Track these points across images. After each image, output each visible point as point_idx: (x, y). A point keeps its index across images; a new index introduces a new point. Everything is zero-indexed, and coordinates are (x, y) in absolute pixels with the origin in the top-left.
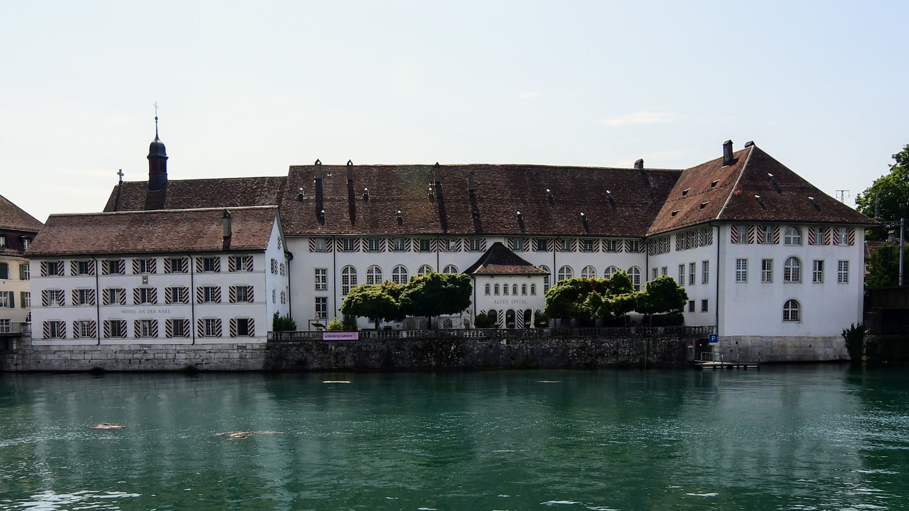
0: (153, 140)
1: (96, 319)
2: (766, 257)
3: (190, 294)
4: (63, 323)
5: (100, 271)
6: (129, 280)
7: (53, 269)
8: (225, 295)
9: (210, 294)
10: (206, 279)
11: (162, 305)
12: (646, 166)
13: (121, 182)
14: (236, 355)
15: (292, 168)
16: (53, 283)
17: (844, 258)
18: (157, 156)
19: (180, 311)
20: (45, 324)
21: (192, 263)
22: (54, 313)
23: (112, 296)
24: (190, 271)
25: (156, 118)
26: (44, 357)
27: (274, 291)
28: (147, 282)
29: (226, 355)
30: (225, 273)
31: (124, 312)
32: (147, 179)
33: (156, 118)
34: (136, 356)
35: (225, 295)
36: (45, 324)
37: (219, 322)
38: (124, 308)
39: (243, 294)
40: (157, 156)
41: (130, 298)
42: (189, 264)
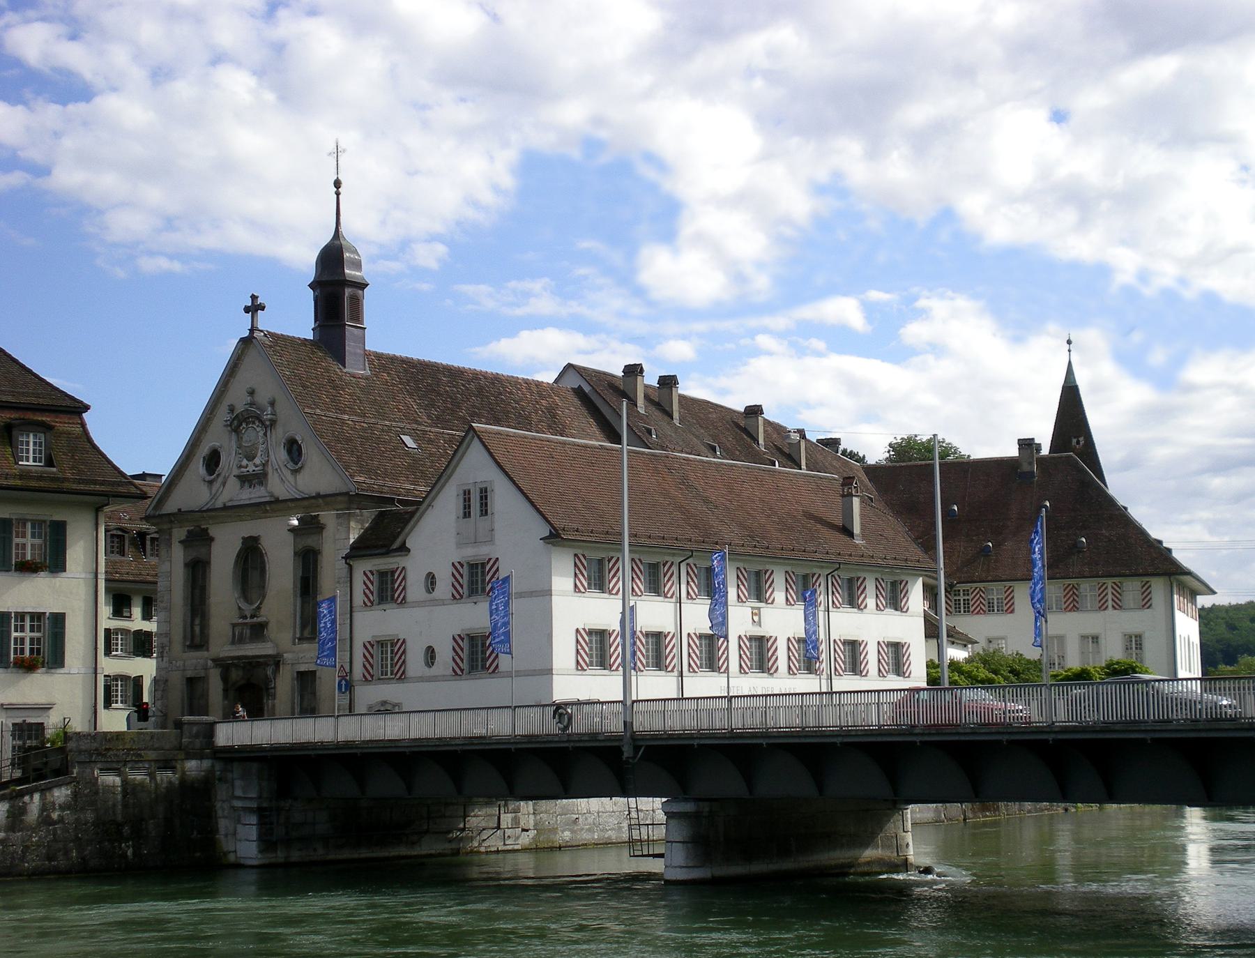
0: (326, 238)
25: (337, 184)
33: (337, 184)
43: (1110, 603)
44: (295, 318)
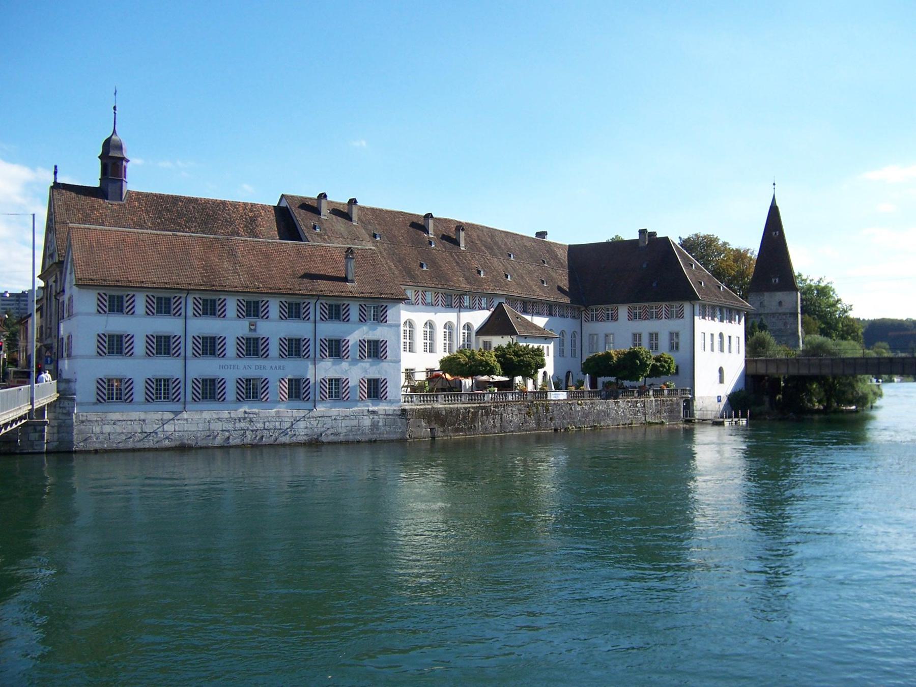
1: (181, 377)
2: (635, 331)
3: (312, 348)
4: (130, 382)
5: (190, 312)
6: (231, 327)
7: (116, 304)
8: (140, 346)
9: (210, 346)
10: (330, 329)
11: (274, 359)
12: (548, 239)
13: (55, 182)
14: (367, 422)
15: (642, 232)
16: (117, 324)
17: (654, 330)
18: (112, 162)
19: (167, 367)
20: (100, 382)
21: (315, 309)
22: (115, 367)
23: (210, 346)
24: (312, 318)
25: (115, 108)
26: (97, 429)
27: (730, 352)
28: (255, 330)
29: (355, 423)
30: (231, 319)
31: (223, 367)
32: (97, 184)
33: (115, 108)
34: (238, 425)
35: (140, 346)
36: (100, 382)
37: (223, 381)
38: (222, 362)
39: (115, 345)
40: (112, 162)
41: (231, 349)
42: (312, 310)
43: (420, 301)
44: (90, 175)
